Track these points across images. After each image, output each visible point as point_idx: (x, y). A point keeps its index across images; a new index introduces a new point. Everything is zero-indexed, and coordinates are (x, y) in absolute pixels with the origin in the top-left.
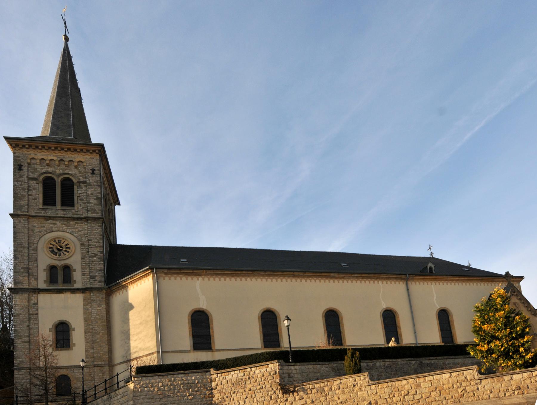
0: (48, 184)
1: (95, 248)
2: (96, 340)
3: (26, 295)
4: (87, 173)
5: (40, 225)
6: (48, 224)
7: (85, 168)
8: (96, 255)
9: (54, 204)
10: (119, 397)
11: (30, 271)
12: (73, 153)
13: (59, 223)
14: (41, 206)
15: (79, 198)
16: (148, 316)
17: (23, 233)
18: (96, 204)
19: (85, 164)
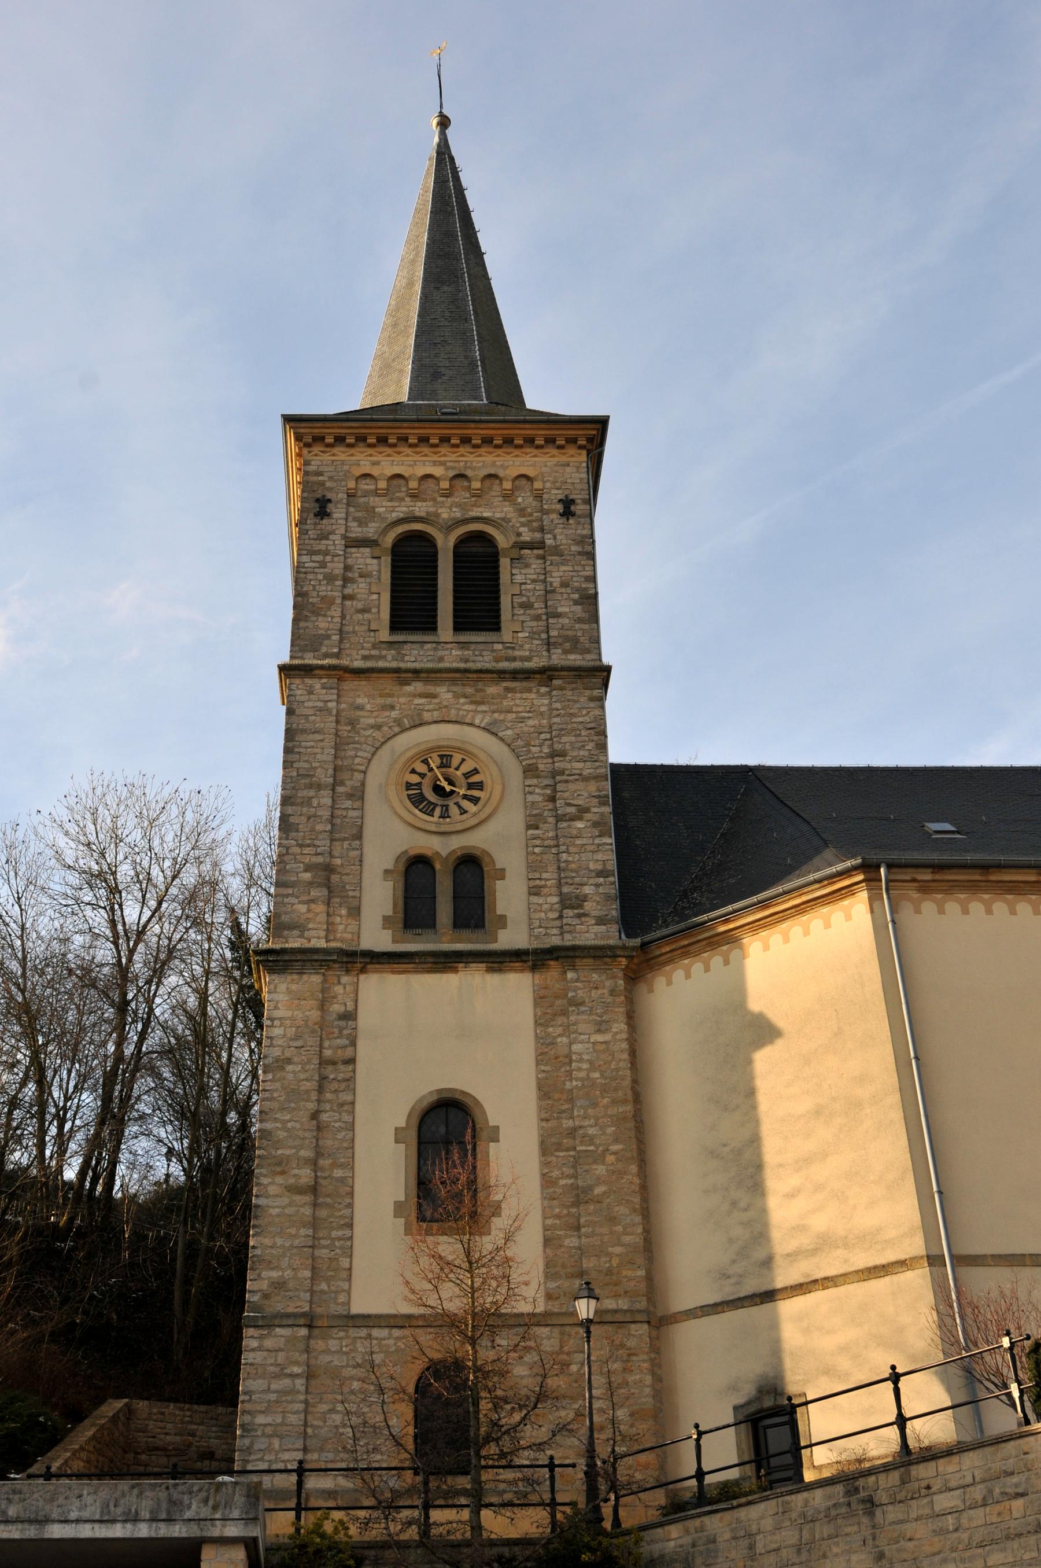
0: (412, 558)
3: (316, 979)
6: (408, 697)
13: (444, 693)
14: (385, 635)
18: (580, 620)
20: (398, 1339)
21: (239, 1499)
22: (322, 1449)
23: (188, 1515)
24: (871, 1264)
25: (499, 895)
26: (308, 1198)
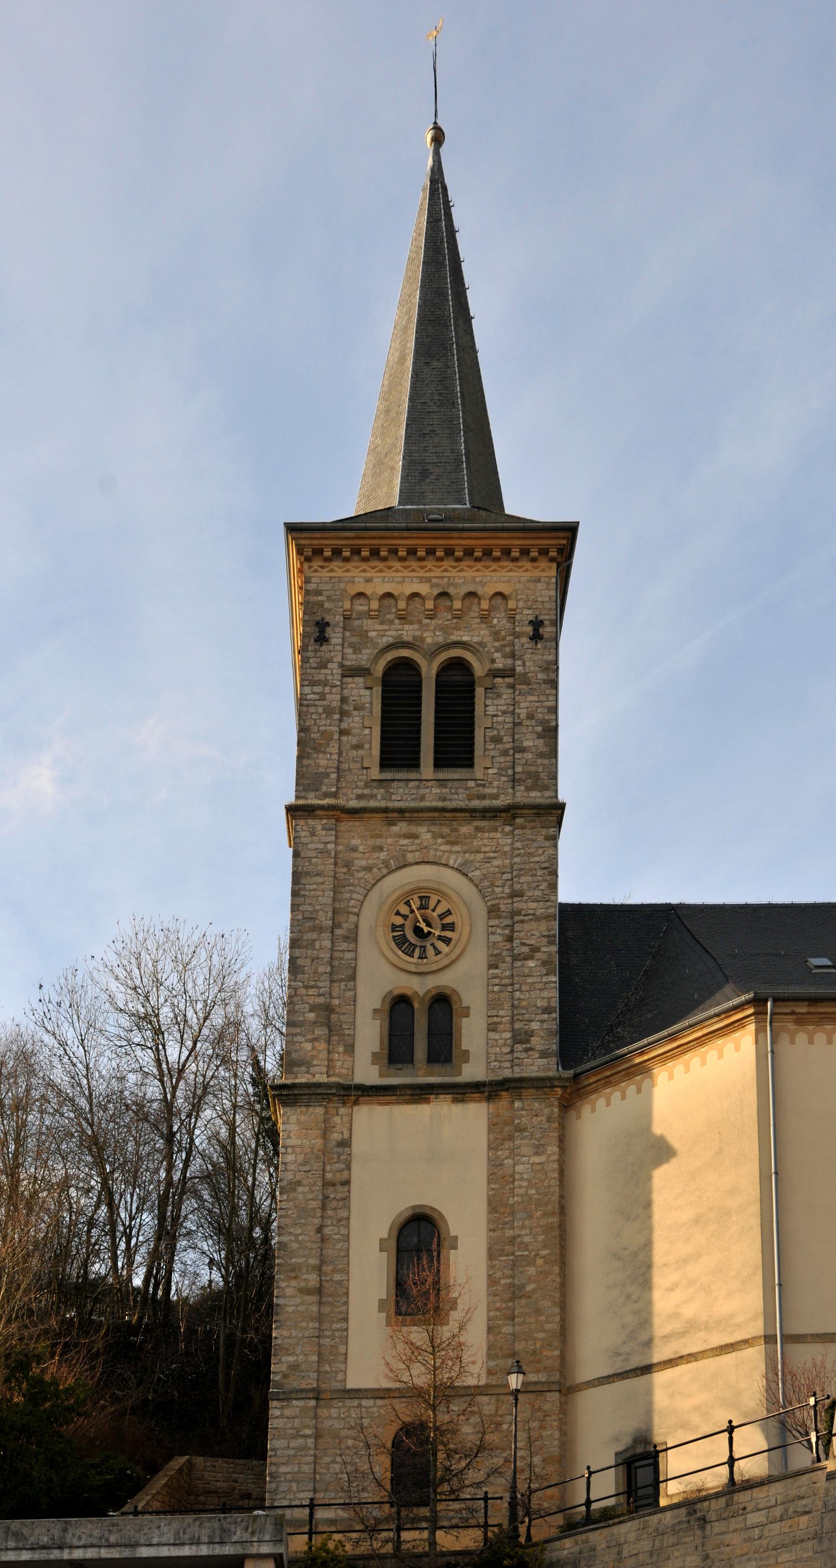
0: (399, 684)
1: (532, 925)
2: (523, 1286)
3: (320, 1111)
4: (517, 635)
5: (371, 842)
7: (512, 618)
8: (535, 949)
9: (414, 763)
10: (754, 1518)
11: (334, 1017)
12: (479, 565)
13: (424, 832)
14: (375, 773)
15: (490, 733)
16: (733, 1192)
17: (318, 874)
19: (512, 604)
20: (380, 1407)
21: (269, 1527)
22: (326, 1490)
23: (234, 1539)
24: (723, 1343)
25: (464, 1031)
26: (315, 1298)
